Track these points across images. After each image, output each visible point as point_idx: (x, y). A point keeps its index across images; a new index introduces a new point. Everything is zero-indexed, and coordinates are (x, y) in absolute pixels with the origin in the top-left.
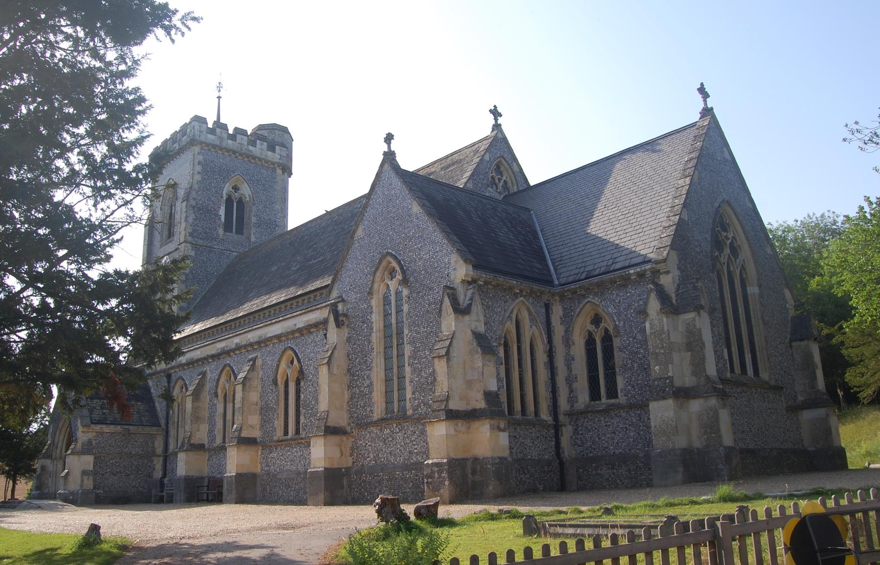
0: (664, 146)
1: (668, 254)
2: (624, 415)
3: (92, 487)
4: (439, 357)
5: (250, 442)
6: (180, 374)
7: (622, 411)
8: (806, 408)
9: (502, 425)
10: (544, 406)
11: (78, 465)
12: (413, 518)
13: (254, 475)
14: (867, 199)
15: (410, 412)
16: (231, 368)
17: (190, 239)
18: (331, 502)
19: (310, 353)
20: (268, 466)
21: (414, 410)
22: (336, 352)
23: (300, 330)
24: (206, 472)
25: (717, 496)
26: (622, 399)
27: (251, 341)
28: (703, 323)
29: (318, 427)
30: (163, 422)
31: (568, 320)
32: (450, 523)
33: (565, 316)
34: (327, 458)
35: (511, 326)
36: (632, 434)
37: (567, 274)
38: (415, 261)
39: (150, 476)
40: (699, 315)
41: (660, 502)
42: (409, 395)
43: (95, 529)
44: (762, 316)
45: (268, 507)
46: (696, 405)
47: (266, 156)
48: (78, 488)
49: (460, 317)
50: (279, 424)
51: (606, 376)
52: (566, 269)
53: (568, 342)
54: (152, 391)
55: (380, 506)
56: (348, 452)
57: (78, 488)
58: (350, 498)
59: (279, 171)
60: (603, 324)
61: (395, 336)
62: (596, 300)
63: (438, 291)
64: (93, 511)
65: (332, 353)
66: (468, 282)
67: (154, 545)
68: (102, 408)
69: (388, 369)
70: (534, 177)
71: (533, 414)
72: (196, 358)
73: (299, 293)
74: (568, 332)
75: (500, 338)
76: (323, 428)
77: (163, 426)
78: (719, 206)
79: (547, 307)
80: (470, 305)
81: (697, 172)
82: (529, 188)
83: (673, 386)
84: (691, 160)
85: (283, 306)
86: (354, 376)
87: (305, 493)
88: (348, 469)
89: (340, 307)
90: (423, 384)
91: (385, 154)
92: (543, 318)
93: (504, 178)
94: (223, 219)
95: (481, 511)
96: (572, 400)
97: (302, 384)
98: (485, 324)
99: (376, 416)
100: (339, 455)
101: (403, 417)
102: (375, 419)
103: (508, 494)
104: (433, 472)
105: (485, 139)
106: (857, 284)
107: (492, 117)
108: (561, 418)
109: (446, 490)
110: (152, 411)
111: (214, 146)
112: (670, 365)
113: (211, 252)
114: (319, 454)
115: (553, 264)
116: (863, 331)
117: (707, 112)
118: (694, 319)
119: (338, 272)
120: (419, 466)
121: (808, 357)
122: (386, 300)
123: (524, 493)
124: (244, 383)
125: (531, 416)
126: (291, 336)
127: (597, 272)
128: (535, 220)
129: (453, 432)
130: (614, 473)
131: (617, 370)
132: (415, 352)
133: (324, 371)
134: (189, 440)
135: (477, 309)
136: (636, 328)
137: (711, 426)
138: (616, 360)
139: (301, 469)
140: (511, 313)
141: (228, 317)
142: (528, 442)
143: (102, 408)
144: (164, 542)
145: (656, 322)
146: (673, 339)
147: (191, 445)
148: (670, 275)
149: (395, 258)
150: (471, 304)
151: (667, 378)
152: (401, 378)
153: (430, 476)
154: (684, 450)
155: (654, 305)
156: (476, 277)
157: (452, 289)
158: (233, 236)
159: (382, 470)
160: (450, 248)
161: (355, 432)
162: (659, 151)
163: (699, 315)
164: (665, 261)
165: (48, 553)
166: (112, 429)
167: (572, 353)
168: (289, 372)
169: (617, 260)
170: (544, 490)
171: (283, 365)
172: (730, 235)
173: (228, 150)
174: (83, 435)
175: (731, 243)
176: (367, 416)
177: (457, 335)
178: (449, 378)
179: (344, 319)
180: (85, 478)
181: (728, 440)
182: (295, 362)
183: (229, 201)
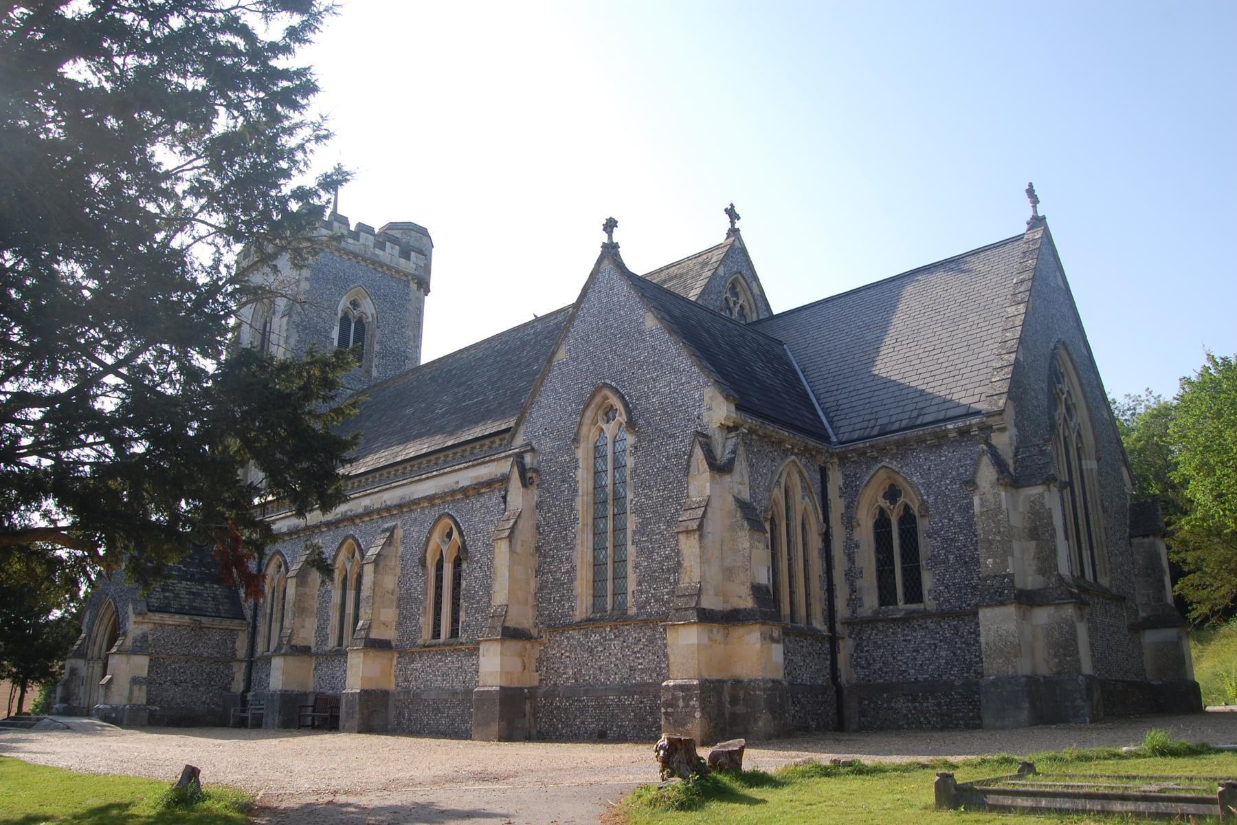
0: (975, 264)
2: (932, 626)
4: (687, 532)
5: (381, 645)
7: (929, 621)
8: (1148, 628)
9: (776, 635)
10: (818, 608)
11: (126, 671)
13: (386, 694)
14: (1211, 358)
15: (632, 611)
16: (356, 541)
18: (509, 735)
19: (479, 522)
20: (406, 680)
21: (639, 608)
22: (521, 524)
23: (464, 490)
24: (311, 685)
25: (1145, 747)
26: (929, 603)
27: (389, 503)
28: (1052, 500)
29: (492, 628)
30: (248, 613)
31: (851, 492)
32: (758, 779)
33: (846, 485)
34: (504, 673)
35: (779, 494)
38: (647, 397)
39: (227, 688)
41: (1068, 752)
42: (631, 586)
43: (191, 773)
46: (1043, 616)
47: (397, 264)
48: (124, 702)
50: (426, 621)
51: (905, 571)
53: (850, 522)
56: (534, 664)
57: (124, 702)
58: (534, 732)
59: (413, 286)
60: (902, 499)
62: (895, 465)
64: (149, 736)
65: (516, 522)
66: (728, 427)
67: (293, 803)
68: (164, 590)
69: (598, 548)
70: (779, 305)
73: (449, 443)
74: (851, 508)
76: (500, 629)
77: (249, 619)
78: (1055, 348)
79: (823, 472)
80: (731, 461)
82: (772, 317)
83: (1014, 587)
84: (1022, 281)
85: (424, 460)
86: (545, 557)
88: (533, 690)
89: (528, 459)
90: (655, 571)
91: (604, 246)
92: (816, 488)
93: (741, 302)
94: (336, 343)
97: (464, 566)
100: (520, 668)
101: (621, 617)
102: (577, 618)
104: (675, 698)
105: (717, 247)
107: (727, 218)
108: (838, 627)
112: (1010, 559)
114: (493, 666)
115: (825, 414)
116: (1209, 530)
117: (1038, 222)
118: (1042, 496)
119: (525, 409)
120: (653, 689)
121: (1154, 557)
125: (802, 625)
126: (449, 498)
127: (896, 426)
129: (706, 641)
130: (915, 708)
131: (923, 563)
133: (502, 548)
134: (289, 641)
135: (741, 466)
136: (953, 506)
137: (1064, 646)
138: (922, 550)
139: (458, 686)
143: (164, 590)
144: (311, 799)
145: (990, 497)
146: (1013, 523)
147: (292, 647)
148: (1007, 433)
149: (616, 391)
150: (733, 459)
151: (1005, 576)
152: (620, 562)
155: (987, 474)
157: (706, 436)
159: (587, 691)
160: (703, 379)
162: (969, 271)
164: (1001, 413)
165: (115, 812)
166: (176, 619)
167: (856, 537)
169: (924, 411)
171: (436, 538)
173: (348, 253)
174: (135, 627)
176: (564, 615)
177: (715, 503)
180: (136, 688)
181: (1087, 667)
182: (455, 534)
183: (345, 320)
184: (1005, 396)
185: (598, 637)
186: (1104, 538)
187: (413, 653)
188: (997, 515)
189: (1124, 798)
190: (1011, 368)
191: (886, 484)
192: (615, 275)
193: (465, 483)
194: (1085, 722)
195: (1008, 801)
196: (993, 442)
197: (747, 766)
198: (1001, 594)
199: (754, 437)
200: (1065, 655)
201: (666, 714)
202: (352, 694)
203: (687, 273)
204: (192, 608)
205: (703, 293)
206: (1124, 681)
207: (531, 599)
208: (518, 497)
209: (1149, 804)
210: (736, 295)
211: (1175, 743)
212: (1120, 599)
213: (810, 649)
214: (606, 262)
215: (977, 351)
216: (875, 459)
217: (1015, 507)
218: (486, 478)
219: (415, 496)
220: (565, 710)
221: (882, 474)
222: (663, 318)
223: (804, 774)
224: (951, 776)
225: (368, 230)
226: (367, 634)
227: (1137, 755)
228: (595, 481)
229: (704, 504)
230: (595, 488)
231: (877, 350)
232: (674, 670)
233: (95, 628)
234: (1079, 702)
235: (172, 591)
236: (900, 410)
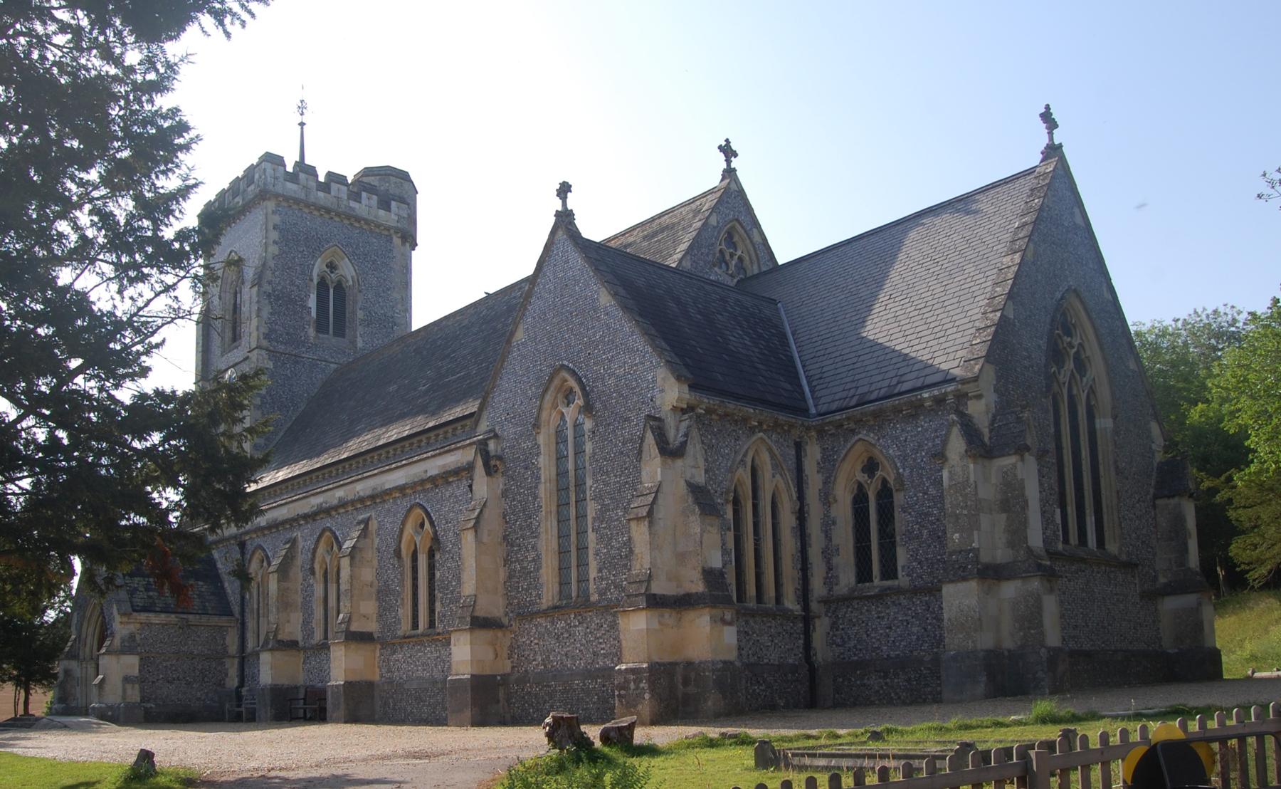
0: (984, 204)
1: (981, 370)
2: (904, 602)
3: (138, 700)
4: (638, 519)
5: (364, 638)
7: (902, 597)
9: (728, 617)
11: (116, 671)
12: (598, 744)
13: (371, 685)
15: (594, 598)
17: (265, 343)
18: (482, 720)
20: (389, 671)
21: (600, 595)
22: (486, 512)
23: (433, 479)
24: (301, 679)
26: (903, 580)
27: (362, 494)
28: (1028, 472)
31: (829, 466)
32: (650, 751)
36: (915, 629)
38: (603, 379)
39: (221, 684)
40: (1022, 460)
42: (593, 573)
43: (146, 756)
44: (1116, 462)
45: (392, 728)
46: (1010, 590)
48: (119, 700)
49: (669, 461)
50: (405, 613)
53: (827, 498)
56: (506, 652)
57: (119, 700)
59: (397, 241)
61: (572, 489)
62: (872, 438)
64: (142, 732)
67: (232, 778)
68: (147, 590)
69: (563, 536)
70: (783, 256)
71: (773, 601)
72: (280, 519)
73: (431, 425)
74: (828, 482)
75: (727, 493)
76: (468, 619)
77: (237, 615)
79: (799, 447)
80: (684, 445)
81: (1031, 246)
83: (978, 562)
85: (407, 444)
86: (512, 546)
87: (444, 709)
89: (492, 445)
90: (614, 558)
91: (558, 214)
92: (792, 463)
93: (739, 253)
94: (314, 314)
96: (830, 581)
97: (437, 556)
98: (706, 471)
100: (491, 656)
101: (584, 604)
102: (544, 607)
104: (627, 681)
107: (722, 157)
108: (814, 606)
110: (220, 593)
111: (297, 201)
113: (297, 362)
114: (463, 655)
116: (1261, 485)
117: (1053, 151)
118: (1014, 466)
119: (487, 393)
120: (608, 673)
121: (1179, 519)
122: (560, 436)
125: (770, 603)
126: (419, 488)
127: (874, 396)
128: (784, 317)
129: (656, 626)
131: (898, 538)
133: (469, 537)
134: (275, 636)
135: (695, 450)
136: (929, 479)
137: (1030, 618)
139: (437, 675)
140: (745, 455)
141: (326, 459)
142: (765, 639)
145: (958, 470)
147: (279, 641)
148: (983, 401)
149: (574, 373)
150: (686, 442)
151: (970, 551)
152: (582, 549)
155: (957, 445)
157: (659, 419)
158: (330, 339)
162: (976, 212)
163: (1022, 460)
164: (975, 379)
168: (418, 539)
172: (1076, 342)
173: (319, 208)
174: (121, 628)
175: (1077, 353)
176: (532, 603)
180: (129, 686)
182: (427, 524)
183: (322, 286)
184: (982, 361)
185: (563, 624)
191: (865, 458)
192: (570, 247)
193: (433, 472)
198: (965, 568)
199: (714, 417)
201: (619, 696)
203: (679, 223)
208: (482, 486)
212: (1130, 566)
213: (780, 630)
214: (560, 233)
215: (966, 308)
216: (853, 431)
219: (387, 487)
220: (536, 695)
221: (859, 447)
223: (689, 746)
225: (341, 179)
226: (348, 627)
228: (558, 468)
230: (558, 475)
232: (626, 654)
236: (880, 377)
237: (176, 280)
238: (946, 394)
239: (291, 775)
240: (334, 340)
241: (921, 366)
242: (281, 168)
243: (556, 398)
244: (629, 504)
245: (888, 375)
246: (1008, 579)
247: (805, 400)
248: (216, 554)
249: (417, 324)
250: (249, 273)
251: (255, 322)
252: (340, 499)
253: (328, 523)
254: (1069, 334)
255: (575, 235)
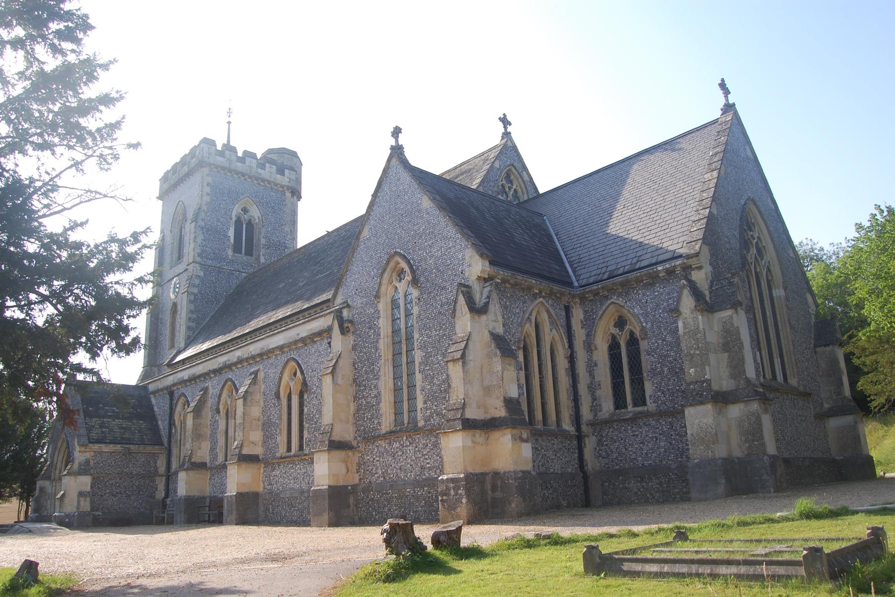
0: (684, 144)
1: (700, 248)
2: (653, 423)
3: (89, 509)
4: (454, 361)
5: (252, 459)
6: (183, 390)
7: (651, 419)
8: (832, 416)
9: (525, 436)
11: (73, 488)
12: (430, 547)
13: (256, 495)
14: (878, 207)
15: (421, 424)
17: (198, 259)
18: (337, 521)
21: (426, 421)
23: (303, 340)
24: (208, 491)
25: (796, 512)
26: (651, 406)
27: (253, 353)
28: (740, 321)
30: (165, 440)
31: (590, 323)
32: (474, 553)
35: (530, 329)
36: (662, 444)
37: (588, 275)
38: (426, 260)
39: (152, 496)
40: (737, 313)
41: (731, 519)
42: (420, 404)
43: (30, 567)
44: (789, 320)
45: (268, 528)
46: (735, 411)
49: (477, 317)
50: (282, 439)
52: (586, 271)
53: (589, 346)
54: (156, 409)
55: (388, 533)
56: (355, 467)
57: (75, 510)
58: (356, 518)
59: (288, 194)
61: (404, 342)
62: (621, 301)
63: (451, 291)
65: (337, 361)
66: (485, 279)
67: (97, 588)
68: (101, 427)
69: (397, 377)
70: (543, 187)
71: (555, 424)
72: (198, 373)
73: (305, 307)
75: (519, 342)
76: (327, 442)
77: (166, 444)
78: (745, 203)
79: (567, 309)
80: (487, 304)
81: (723, 167)
82: (539, 196)
83: (711, 390)
84: (716, 154)
86: (360, 386)
87: (309, 513)
88: (354, 487)
89: (345, 313)
91: (392, 148)
92: (563, 321)
93: (514, 187)
94: (232, 240)
95: (513, 537)
96: (595, 408)
97: (306, 397)
98: (504, 326)
99: (384, 429)
100: (344, 471)
101: (414, 429)
102: (383, 431)
103: (532, 512)
104: (448, 489)
106: (870, 293)
107: (501, 125)
108: (584, 428)
109: (463, 509)
110: (155, 429)
111: (223, 168)
112: (707, 368)
113: (220, 272)
114: (324, 471)
115: (571, 266)
116: (880, 338)
117: (729, 108)
118: (731, 317)
120: (432, 482)
121: (834, 362)
122: (394, 304)
123: (547, 509)
124: (245, 398)
125: (553, 427)
126: (294, 347)
127: (621, 271)
128: (549, 224)
129: (470, 443)
130: (643, 487)
131: (645, 375)
132: (427, 356)
133: (328, 381)
134: (190, 459)
135: (495, 308)
136: (665, 329)
137: (753, 433)
138: (644, 365)
139: (305, 487)
140: (530, 314)
141: (235, 334)
142: (550, 453)
143: (101, 427)
145: (690, 320)
146: (708, 340)
148: (703, 271)
149: (404, 257)
150: (488, 302)
151: (704, 381)
152: (411, 386)
153: (445, 493)
154: (725, 459)
155: (687, 302)
156: (492, 273)
158: (242, 257)
159: (391, 487)
160: (464, 243)
161: (362, 447)
163: (737, 313)
164: (697, 255)
166: (110, 448)
167: (595, 358)
168: (292, 384)
170: (569, 506)
171: (286, 377)
172: (756, 236)
173: (237, 173)
174: (80, 455)
175: (756, 243)
176: (375, 429)
177: (473, 337)
178: (465, 384)
179: (349, 325)
180: (82, 499)
182: (299, 373)
183: (238, 223)
185: (398, 445)
186: (791, 349)
187: (273, 464)
188: (696, 335)
189: (729, 562)
190: (705, 220)
191: (616, 316)
193: (303, 334)
194: (770, 492)
195: (638, 567)
196: (693, 278)
197: (465, 542)
198: (701, 395)
200: (753, 441)
201: (442, 500)
202: (231, 496)
204: (123, 438)
205: (483, 181)
206: (811, 458)
207: (351, 418)
208: (338, 342)
209: (748, 567)
210: (511, 182)
211: (819, 508)
212: (806, 395)
216: (606, 297)
217: (710, 328)
218: (317, 330)
219: (271, 347)
221: (612, 309)
222: (434, 199)
223: (510, 547)
224: (596, 548)
225: (253, 155)
226: (240, 451)
227: (786, 519)
228: (393, 327)
229: (466, 338)
231: (610, 215)
232: (447, 468)
233: (56, 457)
234: (765, 477)
235: (107, 427)
236: (624, 258)
237: (84, 158)
238: (675, 266)
239: (151, 583)
240: (245, 258)
241: (654, 249)
242: (213, 147)
243: (391, 276)
244: (446, 350)
245: (629, 257)
246: (734, 402)
247: (570, 277)
248: (153, 401)
249: (300, 244)
250: (190, 215)
251: (192, 246)
252: (238, 358)
253: (230, 375)
254: (751, 230)
255: (405, 163)
